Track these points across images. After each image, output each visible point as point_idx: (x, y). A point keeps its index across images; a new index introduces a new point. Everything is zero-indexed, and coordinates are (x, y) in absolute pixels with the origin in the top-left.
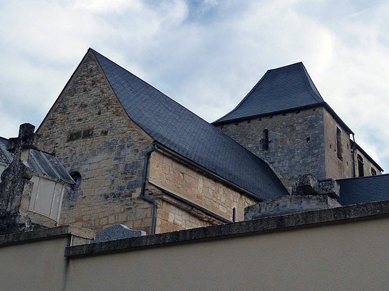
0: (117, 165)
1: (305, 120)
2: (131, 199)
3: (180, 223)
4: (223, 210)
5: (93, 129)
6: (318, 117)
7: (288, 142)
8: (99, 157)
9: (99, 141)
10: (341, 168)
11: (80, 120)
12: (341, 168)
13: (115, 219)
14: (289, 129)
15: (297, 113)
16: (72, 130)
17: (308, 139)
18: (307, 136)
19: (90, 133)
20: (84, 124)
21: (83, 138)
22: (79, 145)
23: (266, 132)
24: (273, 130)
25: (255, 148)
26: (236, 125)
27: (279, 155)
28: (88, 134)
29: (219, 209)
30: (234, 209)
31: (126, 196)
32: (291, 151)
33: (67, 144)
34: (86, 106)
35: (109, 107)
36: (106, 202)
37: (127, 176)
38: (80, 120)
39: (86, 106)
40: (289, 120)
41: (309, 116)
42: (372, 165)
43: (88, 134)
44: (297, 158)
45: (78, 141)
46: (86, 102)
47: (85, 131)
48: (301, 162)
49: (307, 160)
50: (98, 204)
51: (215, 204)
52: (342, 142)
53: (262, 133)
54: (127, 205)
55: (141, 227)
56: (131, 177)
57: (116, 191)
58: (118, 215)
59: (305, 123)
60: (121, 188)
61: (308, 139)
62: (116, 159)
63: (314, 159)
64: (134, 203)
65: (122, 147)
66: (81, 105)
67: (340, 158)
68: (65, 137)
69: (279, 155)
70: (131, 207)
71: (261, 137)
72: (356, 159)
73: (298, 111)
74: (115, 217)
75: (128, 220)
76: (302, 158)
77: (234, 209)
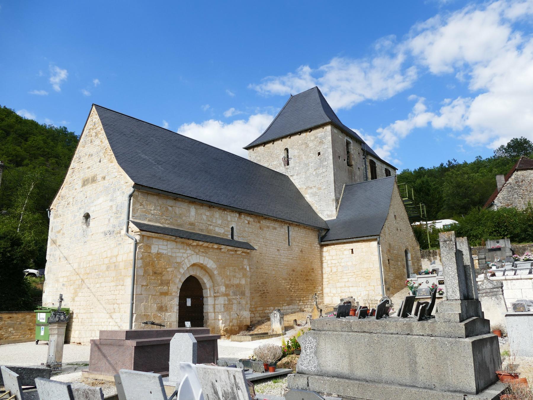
0: (111, 206)
1: (316, 138)
2: (120, 236)
3: (165, 252)
4: (220, 231)
5: (96, 175)
6: (326, 134)
7: (304, 157)
8: (101, 200)
9: (100, 185)
10: (351, 174)
11: (89, 168)
12: (351, 174)
13: (111, 253)
14: (304, 146)
15: (310, 132)
16: (84, 177)
17: (319, 154)
18: (318, 151)
19: (95, 179)
20: (91, 171)
21: (91, 183)
22: (89, 188)
23: (287, 150)
24: (291, 148)
25: (279, 164)
26: (264, 146)
27: (297, 168)
28: (94, 180)
29: (215, 230)
30: (232, 228)
31: (117, 233)
32: (307, 165)
33: (81, 189)
34: (92, 155)
35: (106, 155)
36: (106, 239)
37: (118, 216)
38: (89, 168)
39: (92, 155)
40: (304, 138)
41: (319, 133)
42: (385, 167)
43: (94, 180)
44: (311, 170)
45: (88, 187)
46: (92, 152)
47: (92, 177)
48: (314, 173)
49: (319, 172)
50: (100, 241)
51: (211, 227)
52: (352, 152)
53: (283, 151)
54: (118, 241)
55: (127, 260)
56: (120, 216)
57: (111, 229)
58: (113, 250)
59: (316, 140)
60: (114, 226)
61: (319, 154)
62: (111, 200)
63: (324, 170)
64: (122, 239)
65: (114, 190)
66: (89, 155)
67: (349, 164)
68: (80, 183)
69: (297, 168)
70: (121, 242)
71: (283, 154)
72: (368, 164)
73: (299, 134)
74: (111, 251)
75: (119, 254)
76: (315, 170)
77: (232, 228)
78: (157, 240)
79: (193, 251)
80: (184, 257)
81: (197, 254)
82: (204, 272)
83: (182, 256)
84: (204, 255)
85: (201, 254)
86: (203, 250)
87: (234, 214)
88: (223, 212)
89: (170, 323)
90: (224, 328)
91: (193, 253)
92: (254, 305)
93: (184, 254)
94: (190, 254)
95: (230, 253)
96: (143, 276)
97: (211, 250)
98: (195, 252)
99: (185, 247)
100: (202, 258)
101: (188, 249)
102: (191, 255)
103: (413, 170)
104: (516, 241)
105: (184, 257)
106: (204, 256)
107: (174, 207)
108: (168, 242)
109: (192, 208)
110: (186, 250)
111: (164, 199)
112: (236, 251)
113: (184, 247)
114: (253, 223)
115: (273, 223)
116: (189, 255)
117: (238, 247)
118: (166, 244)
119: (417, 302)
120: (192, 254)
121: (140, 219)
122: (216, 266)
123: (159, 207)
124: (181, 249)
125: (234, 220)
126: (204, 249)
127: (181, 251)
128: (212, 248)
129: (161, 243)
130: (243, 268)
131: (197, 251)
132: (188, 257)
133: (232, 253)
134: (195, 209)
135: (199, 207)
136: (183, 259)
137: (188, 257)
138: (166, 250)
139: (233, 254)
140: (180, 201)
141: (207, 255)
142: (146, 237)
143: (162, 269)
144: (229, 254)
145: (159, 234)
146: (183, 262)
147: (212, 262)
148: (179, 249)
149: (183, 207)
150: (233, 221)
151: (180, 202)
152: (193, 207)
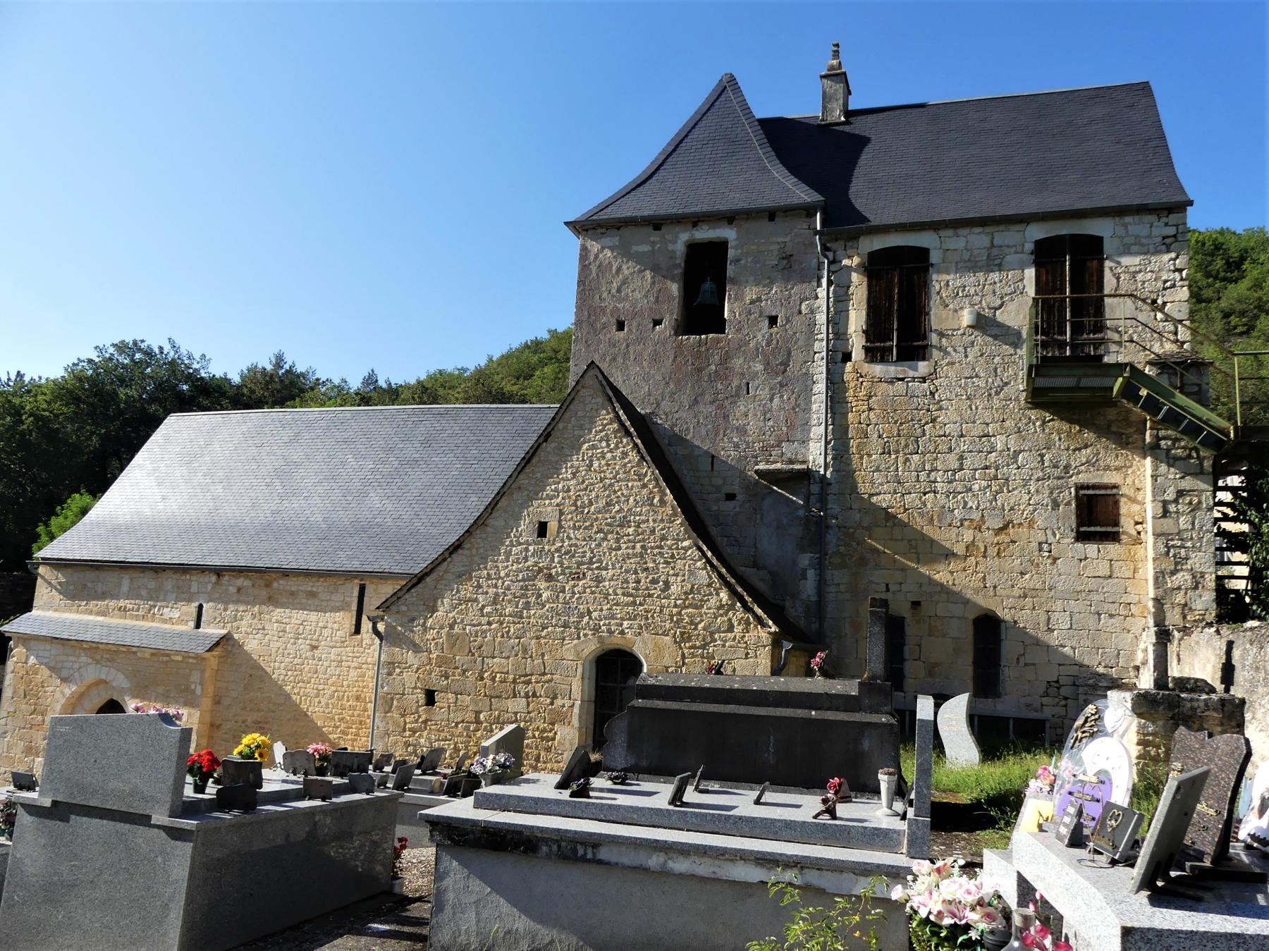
81: (98, 662)
84: (108, 663)
85: (104, 664)
86: (108, 656)
87: (207, 576)
88: (183, 578)
91: (90, 660)
96: (13, 698)
98: (94, 660)
99: (77, 652)
100: (105, 670)
103: (472, 368)
104: (458, 795)
106: (110, 667)
110: (78, 657)
115: (311, 584)
116: (82, 665)
119: (662, 860)
120: (89, 664)
122: (128, 685)
125: (204, 590)
130: (187, 689)
132: (80, 668)
135: (137, 575)
136: (71, 672)
137: (80, 668)
147: (123, 676)
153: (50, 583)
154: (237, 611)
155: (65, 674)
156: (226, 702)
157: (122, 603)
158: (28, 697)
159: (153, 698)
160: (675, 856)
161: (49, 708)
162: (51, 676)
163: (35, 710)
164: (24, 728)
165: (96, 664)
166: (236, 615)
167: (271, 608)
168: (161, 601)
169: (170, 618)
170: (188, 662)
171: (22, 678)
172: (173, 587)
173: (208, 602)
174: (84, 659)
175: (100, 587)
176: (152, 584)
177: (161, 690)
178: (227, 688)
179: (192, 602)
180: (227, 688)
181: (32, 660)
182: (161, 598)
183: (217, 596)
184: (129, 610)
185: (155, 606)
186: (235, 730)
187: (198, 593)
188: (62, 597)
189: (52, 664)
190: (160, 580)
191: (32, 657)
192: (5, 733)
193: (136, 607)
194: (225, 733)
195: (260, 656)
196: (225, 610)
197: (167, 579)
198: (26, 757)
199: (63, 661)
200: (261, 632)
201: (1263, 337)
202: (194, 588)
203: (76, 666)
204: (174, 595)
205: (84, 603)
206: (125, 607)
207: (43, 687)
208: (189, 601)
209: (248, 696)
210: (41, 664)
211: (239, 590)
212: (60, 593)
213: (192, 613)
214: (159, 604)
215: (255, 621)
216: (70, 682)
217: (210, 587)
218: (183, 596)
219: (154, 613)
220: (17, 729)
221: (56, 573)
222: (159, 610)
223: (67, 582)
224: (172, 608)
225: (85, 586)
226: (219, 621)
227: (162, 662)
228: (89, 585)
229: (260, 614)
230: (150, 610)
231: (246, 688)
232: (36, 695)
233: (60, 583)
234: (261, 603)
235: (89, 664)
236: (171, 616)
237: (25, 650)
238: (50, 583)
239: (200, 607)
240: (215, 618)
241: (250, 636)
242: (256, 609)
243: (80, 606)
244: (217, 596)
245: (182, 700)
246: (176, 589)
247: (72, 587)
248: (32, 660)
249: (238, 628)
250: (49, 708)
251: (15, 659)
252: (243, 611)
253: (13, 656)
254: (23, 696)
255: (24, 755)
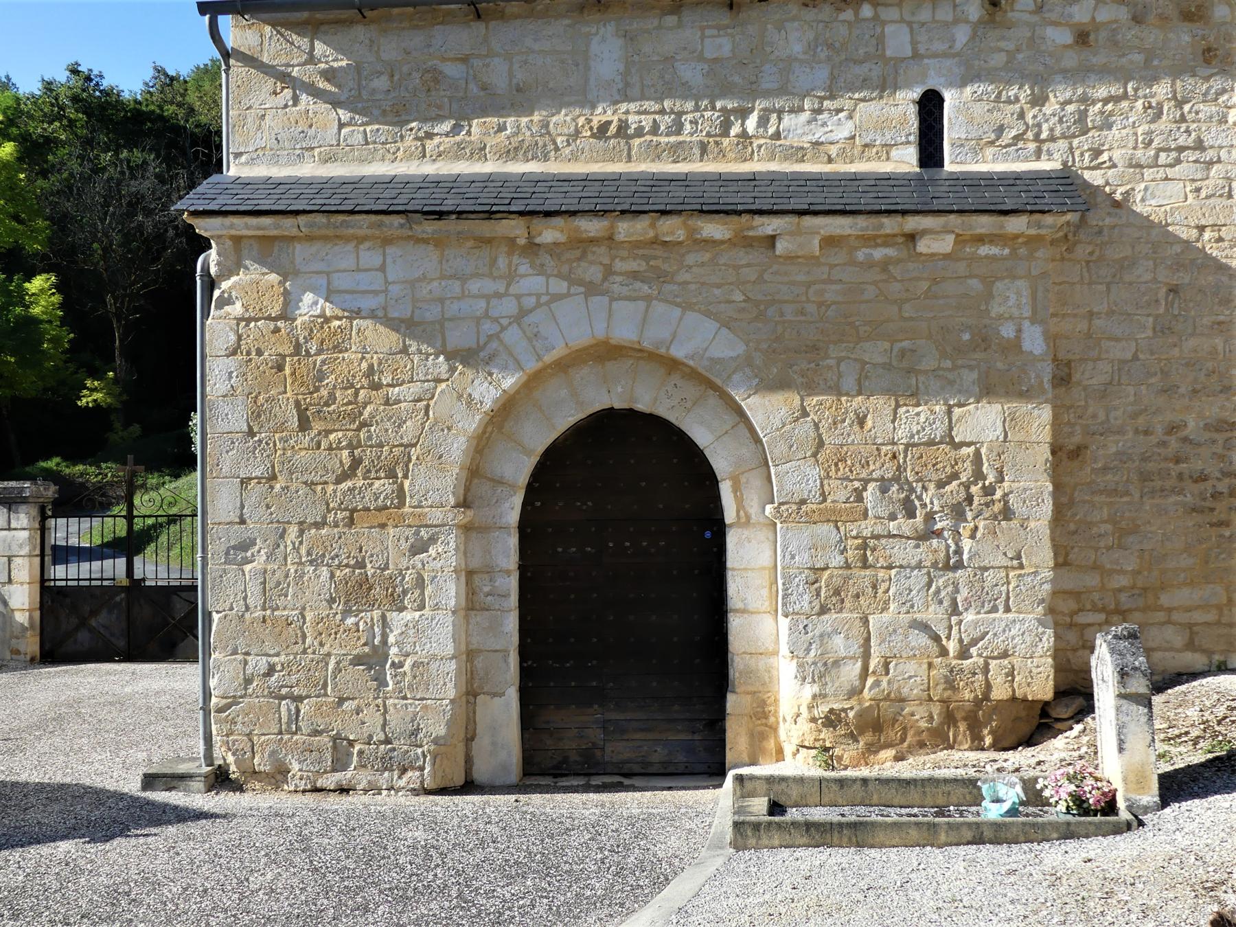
78: (316, 247)
79: (560, 276)
80: (496, 320)
81: (592, 289)
82: (691, 390)
83: (486, 315)
85: (625, 291)
86: (633, 265)
88: (848, 15)
89: (415, 665)
90: (810, 708)
91: (560, 286)
92: (1137, 573)
93: (494, 302)
94: (538, 296)
95: (860, 255)
96: (251, 433)
97: (690, 259)
98: (572, 282)
99: (502, 262)
101: (523, 269)
102: (548, 303)
105: (496, 320)
106: (648, 299)
107: (477, 63)
108: (391, 250)
109: (604, 40)
111: (416, 27)
112: (912, 237)
113: (494, 262)
114: (1130, 34)
117: (904, 213)
118: (377, 260)
120: (557, 298)
121: (275, 160)
122: (740, 349)
123: (384, 78)
124: (477, 275)
125: (939, 46)
126: (646, 258)
127: (474, 286)
128: (532, 248)
129: (348, 262)
130: (984, 340)
131: (593, 273)
132: (523, 313)
133: (879, 253)
134: (621, 42)
136: (488, 327)
137: (523, 313)
138: (375, 293)
139: (885, 265)
140: (517, 17)
141: (668, 288)
142: (252, 241)
143: (356, 394)
144: (853, 263)
145: (302, 219)
146: (494, 345)
148: (463, 279)
149: (537, 47)
150: (935, 56)
151: (518, 22)
152: (611, 28)
153: (284, 78)
154: (1084, 99)
155: (459, 337)
156: (1092, 376)
157: (604, 113)
158: (317, 426)
159: (849, 382)
160: (258, 785)
161: (414, 453)
162: (405, 350)
163: (356, 462)
164: (317, 525)
165: (587, 295)
166: (1083, 115)
167: (1217, 83)
168: (766, 94)
169: (817, 144)
170: (974, 258)
171: (280, 368)
172: (812, 47)
173: (963, 84)
174: (531, 283)
175: (499, 75)
176: (721, 45)
177: (875, 352)
178: (1089, 335)
179: (896, 88)
180: (1089, 335)
181: (310, 305)
182: (767, 83)
183: (999, 59)
184: (639, 132)
185: (744, 114)
186: (1144, 459)
187: (916, 56)
188: (344, 115)
189: (401, 311)
190: (752, 29)
191: (308, 298)
192: (245, 545)
193: (668, 119)
194: (1105, 469)
195: (1201, 229)
196: (1038, 101)
197: (780, 27)
198: (347, 613)
199: (442, 301)
200: (1192, 156)
201: (403, 325)
202: (898, 41)
203: (508, 307)
204: (823, 73)
205: (446, 126)
206: (623, 127)
207: (376, 386)
208: (885, 85)
209: (1176, 352)
210: (357, 314)
211: (1082, 37)
212: (336, 104)
213: (904, 121)
214: (760, 104)
215: (1164, 124)
216: (489, 360)
217: (962, 35)
218: (861, 70)
219: (744, 135)
220: (293, 531)
221: (304, 42)
222: (763, 122)
223: (358, 68)
224: (819, 111)
225: (435, 78)
226: (1017, 138)
227: (870, 264)
228: (452, 70)
229: (1180, 104)
230: (726, 127)
231: (1163, 329)
232: (353, 417)
233: (329, 75)
234: (1176, 72)
235: (557, 298)
236: (819, 135)
237: (274, 278)
238: (284, 78)
239: (930, 106)
240: (1000, 130)
241: (1148, 173)
242: (1162, 90)
243: (429, 136)
244: (999, 59)
245: (970, 377)
246: (823, 54)
247: (382, 83)
248: (310, 305)
249: (1097, 153)
250: (414, 453)
251: (237, 309)
252: (1106, 101)
253: (225, 301)
254: (294, 423)
255: (338, 607)
